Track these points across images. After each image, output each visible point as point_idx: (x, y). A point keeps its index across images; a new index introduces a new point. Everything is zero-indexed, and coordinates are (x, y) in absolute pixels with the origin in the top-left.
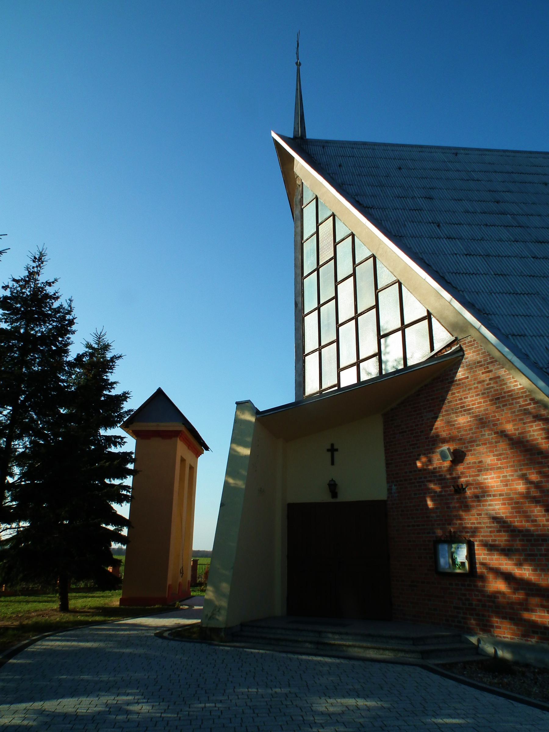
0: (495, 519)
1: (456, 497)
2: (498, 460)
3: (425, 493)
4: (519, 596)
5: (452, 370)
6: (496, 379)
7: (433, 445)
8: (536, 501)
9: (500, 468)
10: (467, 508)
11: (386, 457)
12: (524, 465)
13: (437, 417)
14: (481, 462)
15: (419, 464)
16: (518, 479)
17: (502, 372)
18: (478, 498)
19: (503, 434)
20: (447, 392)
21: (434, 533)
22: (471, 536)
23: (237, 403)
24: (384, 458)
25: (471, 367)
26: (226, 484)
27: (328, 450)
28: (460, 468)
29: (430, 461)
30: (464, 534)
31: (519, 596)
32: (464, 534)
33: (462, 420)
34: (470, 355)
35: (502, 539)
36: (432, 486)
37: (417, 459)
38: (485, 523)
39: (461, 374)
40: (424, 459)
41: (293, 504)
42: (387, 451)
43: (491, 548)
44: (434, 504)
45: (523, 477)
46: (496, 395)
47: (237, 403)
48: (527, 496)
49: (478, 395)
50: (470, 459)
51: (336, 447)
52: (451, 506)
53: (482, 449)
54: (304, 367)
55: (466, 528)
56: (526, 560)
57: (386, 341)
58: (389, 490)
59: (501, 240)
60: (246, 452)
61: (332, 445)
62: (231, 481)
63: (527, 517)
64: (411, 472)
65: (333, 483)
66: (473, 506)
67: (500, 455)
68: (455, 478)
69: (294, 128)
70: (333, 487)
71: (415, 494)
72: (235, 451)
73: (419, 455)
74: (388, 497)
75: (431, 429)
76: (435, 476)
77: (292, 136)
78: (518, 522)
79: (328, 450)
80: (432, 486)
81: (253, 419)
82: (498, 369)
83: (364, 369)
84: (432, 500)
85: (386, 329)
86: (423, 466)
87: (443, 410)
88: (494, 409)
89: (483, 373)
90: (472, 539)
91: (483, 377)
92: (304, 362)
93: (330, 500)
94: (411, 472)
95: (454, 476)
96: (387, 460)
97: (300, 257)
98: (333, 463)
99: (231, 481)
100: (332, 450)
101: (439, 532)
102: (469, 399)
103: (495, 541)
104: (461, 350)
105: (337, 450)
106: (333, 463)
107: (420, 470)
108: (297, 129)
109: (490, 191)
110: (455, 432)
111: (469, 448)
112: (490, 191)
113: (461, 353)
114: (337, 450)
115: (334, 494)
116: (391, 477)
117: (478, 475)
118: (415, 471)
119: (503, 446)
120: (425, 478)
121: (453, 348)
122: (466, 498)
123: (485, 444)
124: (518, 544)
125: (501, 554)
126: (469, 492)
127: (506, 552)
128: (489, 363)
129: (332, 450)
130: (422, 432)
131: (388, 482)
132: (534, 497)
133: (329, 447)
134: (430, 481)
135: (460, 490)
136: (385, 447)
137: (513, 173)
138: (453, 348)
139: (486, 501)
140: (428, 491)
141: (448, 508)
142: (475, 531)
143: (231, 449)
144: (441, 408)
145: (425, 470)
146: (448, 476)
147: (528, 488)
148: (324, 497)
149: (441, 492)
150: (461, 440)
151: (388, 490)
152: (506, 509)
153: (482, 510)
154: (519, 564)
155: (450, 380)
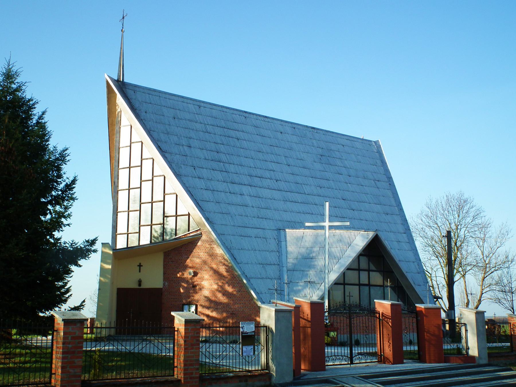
0: (206, 297)
1: (193, 289)
2: (210, 277)
3: (181, 287)
4: (211, 321)
5: (197, 241)
6: (212, 248)
7: (186, 268)
8: (220, 292)
9: (210, 280)
10: (196, 293)
11: (164, 270)
12: (218, 279)
13: (188, 258)
14: (203, 277)
15: (178, 275)
16: (215, 284)
17: (215, 246)
18: (200, 289)
19: (212, 268)
20: (194, 249)
21: (183, 301)
22: (197, 303)
23: (102, 244)
24: (163, 271)
25: (203, 241)
26: (100, 280)
27: (138, 266)
28: (195, 278)
29: (183, 274)
30: (194, 302)
31: (211, 321)
32: (194, 302)
33: (198, 261)
34: (204, 237)
35: (207, 304)
36: (183, 284)
37: (178, 273)
38: (202, 297)
39: (199, 244)
40: (180, 274)
41: (120, 288)
42: (164, 268)
43: (203, 307)
44: (184, 291)
45: (217, 284)
46: (212, 254)
47: (102, 244)
48: (217, 290)
49: (205, 252)
50: (199, 275)
51: (141, 265)
52: (190, 292)
53: (205, 272)
54: (117, 218)
55: (195, 300)
56: (214, 310)
57: (166, 219)
58: (164, 285)
59: (218, 181)
60: (109, 267)
61: (140, 264)
62: (102, 279)
63: (216, 297)
64: (175, 278)
65: (140, 280)
66: (199, 292)
67: (211, 275)
68: (193, 282)
69: (118, 73)
70: (140, 282)
71: (176, 287)
72: (103, 266)
73: (179, 271)
74: (163, 287)
75: (185, 262)
76: (185, 280)
77: (116, 79)
78: (213, 299)
79: (138, 266)
80: (183, 284)
81: (111, 252)
82: (214, 244)
83: (154, 229)
84: (183, 289)
85: (167, 214)
86: (180, 276)
87: (191, 255)
88: (211, 259)
89: (208, 245)
90: (197, 304)
91: (208, 246)
92: (117, 215)
93: (138, 287)
94: (175, 278)
95: (193, 281)
96: (164, 272)
97: (118, 155)
98: (140, 272)
99: (102, 279)
100: (140, 266)
101: (184, 301)
102: (202, 253)
103: (205, 304)
104: (201, 234)
105: (142, 266)
106: (140, 272)
107: (179, 277)
108: (119, 74)
109: (215, 143)
110: (194, 265)
111: (200, 271)
112: (215, 143)
113: (201, 235)
114: (142, 266)
115: (140, 285)
116: (165, 279)
117: (202, 282)
118: (177, 278)
119: (211, 273)
120: (181, 281)
121: (198, 232)
122: (196, 289)
123: (206, 271)
124: (212, 305)
125: (207, 309)
126: (198, 287)
127: (208, 308)
128: (211, 242)
129: (140, 266)
130: (181, 262)
131: (164, 281)
132: (220, 290)
133: (139, 264)
134: (183, 282)
135: (194, 286)
136: (164, 266)
137: (225, 128)
138: (198, 232)
139: (204, 291)
140: (181, 285)
141: (189, 292)
142: (198, 301)
143: (101, 265)
144: (190, 255)
145: (181, 278)
146: (190, 281)
147: (218, 287)
148: (136, 286)
149: (187, 286)
150: (197, 268)
151: (163, 284)
152: (210, 294)
153: (202, 294)
154: (212, 312)
155: (195, 244)
